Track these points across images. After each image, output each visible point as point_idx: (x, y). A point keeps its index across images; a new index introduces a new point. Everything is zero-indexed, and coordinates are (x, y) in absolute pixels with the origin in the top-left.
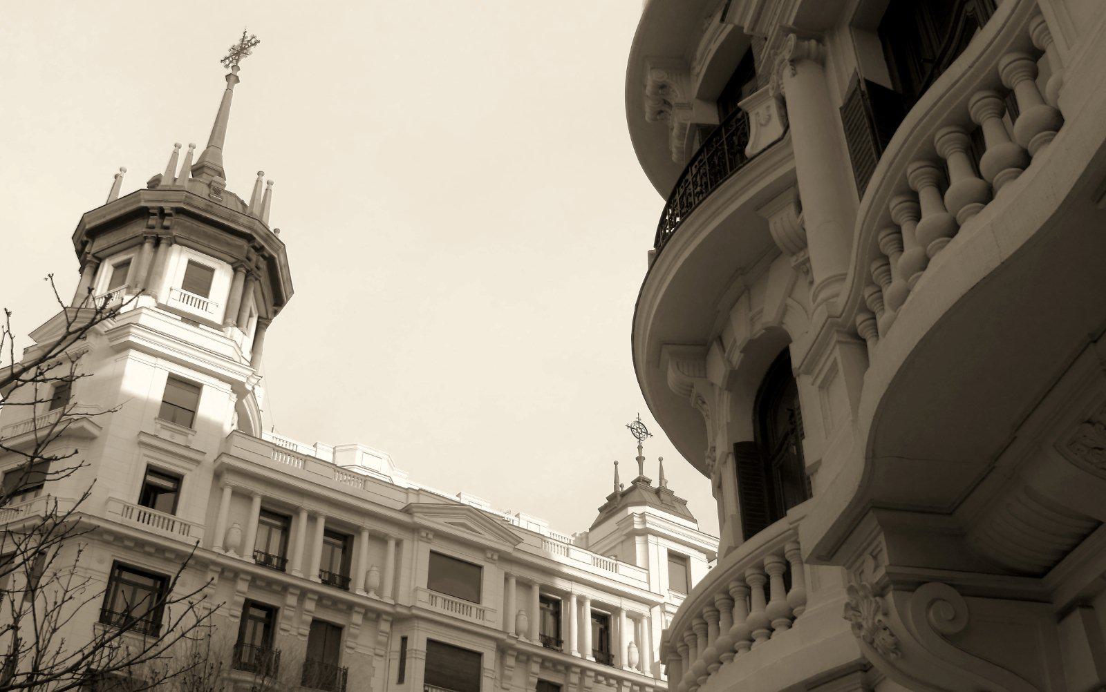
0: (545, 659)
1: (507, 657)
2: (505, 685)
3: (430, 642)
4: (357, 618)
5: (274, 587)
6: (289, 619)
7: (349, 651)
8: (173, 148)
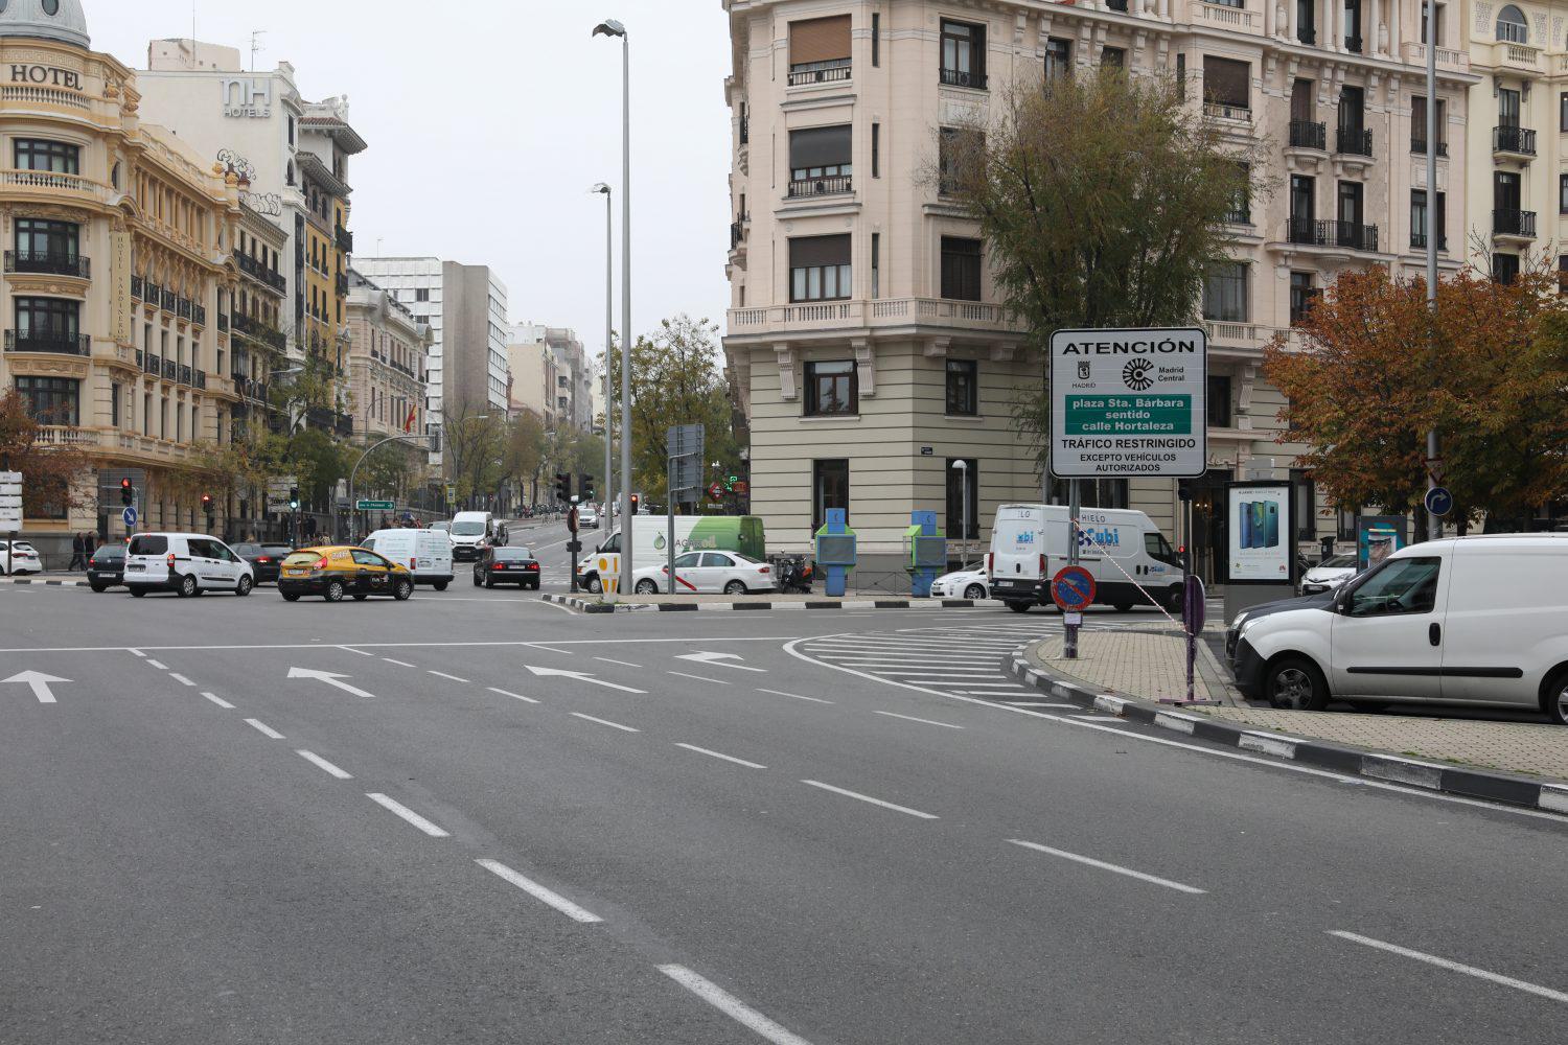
0: (1111, 24)
1: (1043, 22)
2: (1265, 90)
3: (1206, 57)
4: (1141, 42)
5: (1001, 8)
6: (1138, 60)
7: (1079, 66)
8: (1080, 648)
